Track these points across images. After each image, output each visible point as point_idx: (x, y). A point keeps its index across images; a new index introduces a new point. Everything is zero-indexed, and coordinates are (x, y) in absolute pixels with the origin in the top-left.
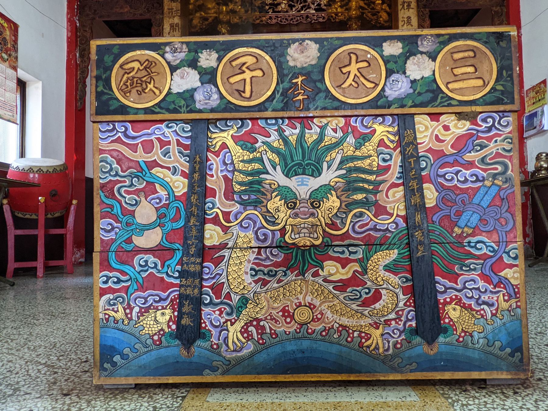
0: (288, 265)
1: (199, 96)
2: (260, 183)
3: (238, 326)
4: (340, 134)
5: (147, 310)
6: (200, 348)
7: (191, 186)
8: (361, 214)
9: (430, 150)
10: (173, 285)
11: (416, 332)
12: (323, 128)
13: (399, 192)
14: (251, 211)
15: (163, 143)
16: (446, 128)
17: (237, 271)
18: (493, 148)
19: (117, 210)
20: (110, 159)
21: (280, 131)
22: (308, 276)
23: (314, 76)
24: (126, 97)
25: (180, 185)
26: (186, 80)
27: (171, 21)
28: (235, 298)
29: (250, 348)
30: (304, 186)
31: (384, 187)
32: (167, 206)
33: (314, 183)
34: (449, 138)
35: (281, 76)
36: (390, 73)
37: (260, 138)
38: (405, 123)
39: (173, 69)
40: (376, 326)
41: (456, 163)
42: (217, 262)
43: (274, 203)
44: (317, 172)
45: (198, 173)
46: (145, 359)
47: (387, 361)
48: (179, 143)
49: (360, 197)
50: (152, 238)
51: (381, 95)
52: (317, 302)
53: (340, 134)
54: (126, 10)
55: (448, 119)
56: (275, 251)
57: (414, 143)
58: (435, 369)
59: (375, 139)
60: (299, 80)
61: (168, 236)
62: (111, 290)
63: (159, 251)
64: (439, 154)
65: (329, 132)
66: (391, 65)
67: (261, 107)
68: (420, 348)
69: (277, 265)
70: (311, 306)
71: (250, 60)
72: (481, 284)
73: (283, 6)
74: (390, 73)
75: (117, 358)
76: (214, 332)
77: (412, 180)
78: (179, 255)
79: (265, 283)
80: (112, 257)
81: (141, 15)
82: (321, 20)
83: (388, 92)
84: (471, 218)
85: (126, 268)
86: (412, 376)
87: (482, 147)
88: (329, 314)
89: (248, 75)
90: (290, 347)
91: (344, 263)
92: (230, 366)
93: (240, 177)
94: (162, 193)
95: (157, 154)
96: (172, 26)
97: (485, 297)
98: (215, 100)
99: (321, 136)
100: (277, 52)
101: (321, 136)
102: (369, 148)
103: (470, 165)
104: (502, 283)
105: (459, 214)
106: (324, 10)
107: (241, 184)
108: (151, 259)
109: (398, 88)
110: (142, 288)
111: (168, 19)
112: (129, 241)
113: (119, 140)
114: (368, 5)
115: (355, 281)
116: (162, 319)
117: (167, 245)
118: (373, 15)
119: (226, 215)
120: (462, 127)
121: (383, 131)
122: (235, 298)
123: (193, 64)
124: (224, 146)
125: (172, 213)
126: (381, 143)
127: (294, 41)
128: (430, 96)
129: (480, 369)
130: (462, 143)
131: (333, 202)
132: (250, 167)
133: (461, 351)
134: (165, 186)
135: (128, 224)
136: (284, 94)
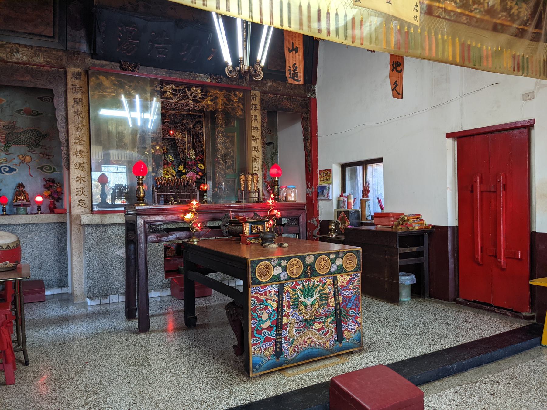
0: (305, 327)
1: (281, 276)
2: (297, 301)
3: (292, 349)
4: (318, 283)
5: (266, 349)
6: (282, 358)
7: (278, 305)
8: (324, 308)
9: (341, 286)
10: (273, 339)
11: (337, 341)
12: (314, 282)
13: (333, 299)
14: (295, 311)
15: (270, 292)
16: (344, 279)
17: (291, 332)
18: (355, 283)
19: (257, 316)
20: (254, 299)
21: (303, 284)
22: (310, 329)
23: (312, 266)
24: (260, 278)
25: (275, 305)
26: (278, 271)
27: (75, 96)
28: (291, 340)
29: (295, 354)
30: (309, 301)
31: (329, 298)
32: (271, 313)
33: (312, 299)
34: (345, 282)
35: (304, 267)
36: (332, 264)
37: (297, 287)
38: (335, 279)
39: (274, 267)
40: (327, 341)
41: (347, 289)
42: (286, 329)
43: (302, 307)
44: (312, 296)
45: (280, 301)
46: (265, 365)
47: (331, 351)
48: (275, 291)
49: (324, 302)
50: (267, 325)
51: (330, 271)
52: (312, 337)
53: (318, 283)
54: (27, 79)
55: (345, 276)
56: (302, 323)
57: (337, 284)
58: (342, 350)
59: (327, 284)
60: (308, 268)
61: (272, 323)
62: (255, 344)
63: (270, 329)
64: (342, 287)
65: (316, 283)
66: (332, 261)
67: (299, 278)
68: (339, 345)
69: (302, 327)
70: (311, 338)
71: (295, 262)
72: (352, 323)
73: (168, 93)
74: (332, 264)
75: (257, 367)
76: (285, 352)
77: (336, 294)
78: (275, 328)
79: (299, 333)
80: (255, 332)
81: (42, 85)
82: (196, 108)
83: (331, 270)
84: (350, 305)
85: (259, 336)
86: (336, 354)
87: (353, 283)
88: (316, 340)
89: (295, 268)
90: (306, 352)
91: (319, 323)
92: (290, 362)
93: (292, 300)
94: (270, 309)
95: (268, 296)
96: (75, 100)
97: (353, 328)
98: (286, 277)
99: (314, 284)
100: (303, 258)
101: (314, 284)
102: (326, 286)
103: (350, 289)
104: (357, 322)
105: (347, 304)
106: (199, 102)
107: (292, 302)
108: (267, 331)
109: (334, 268)
110: (264, 342)
111: (72, 94)
112: (260, 326)
113: (257, 293)
114: (229, 102)
115: (322, 328)
116: (271, 350)
117: (271, 326)
118: (233, 109)
119: (288, 313)
120: (348, 278)
121: (329, 281)
122: (291, 340)
123: (280, 265)
124: (288, 290)
125: (273, 315)
126: (329, 285)
127: (307, 255)
128: (341, 270)
129: (352, 348)
130: (348, 283)
131: (317, 305)
132: (294, 297)
133: (347, 344)
134: (271, 306)
135: (260, 321)
136: (305, 273)
